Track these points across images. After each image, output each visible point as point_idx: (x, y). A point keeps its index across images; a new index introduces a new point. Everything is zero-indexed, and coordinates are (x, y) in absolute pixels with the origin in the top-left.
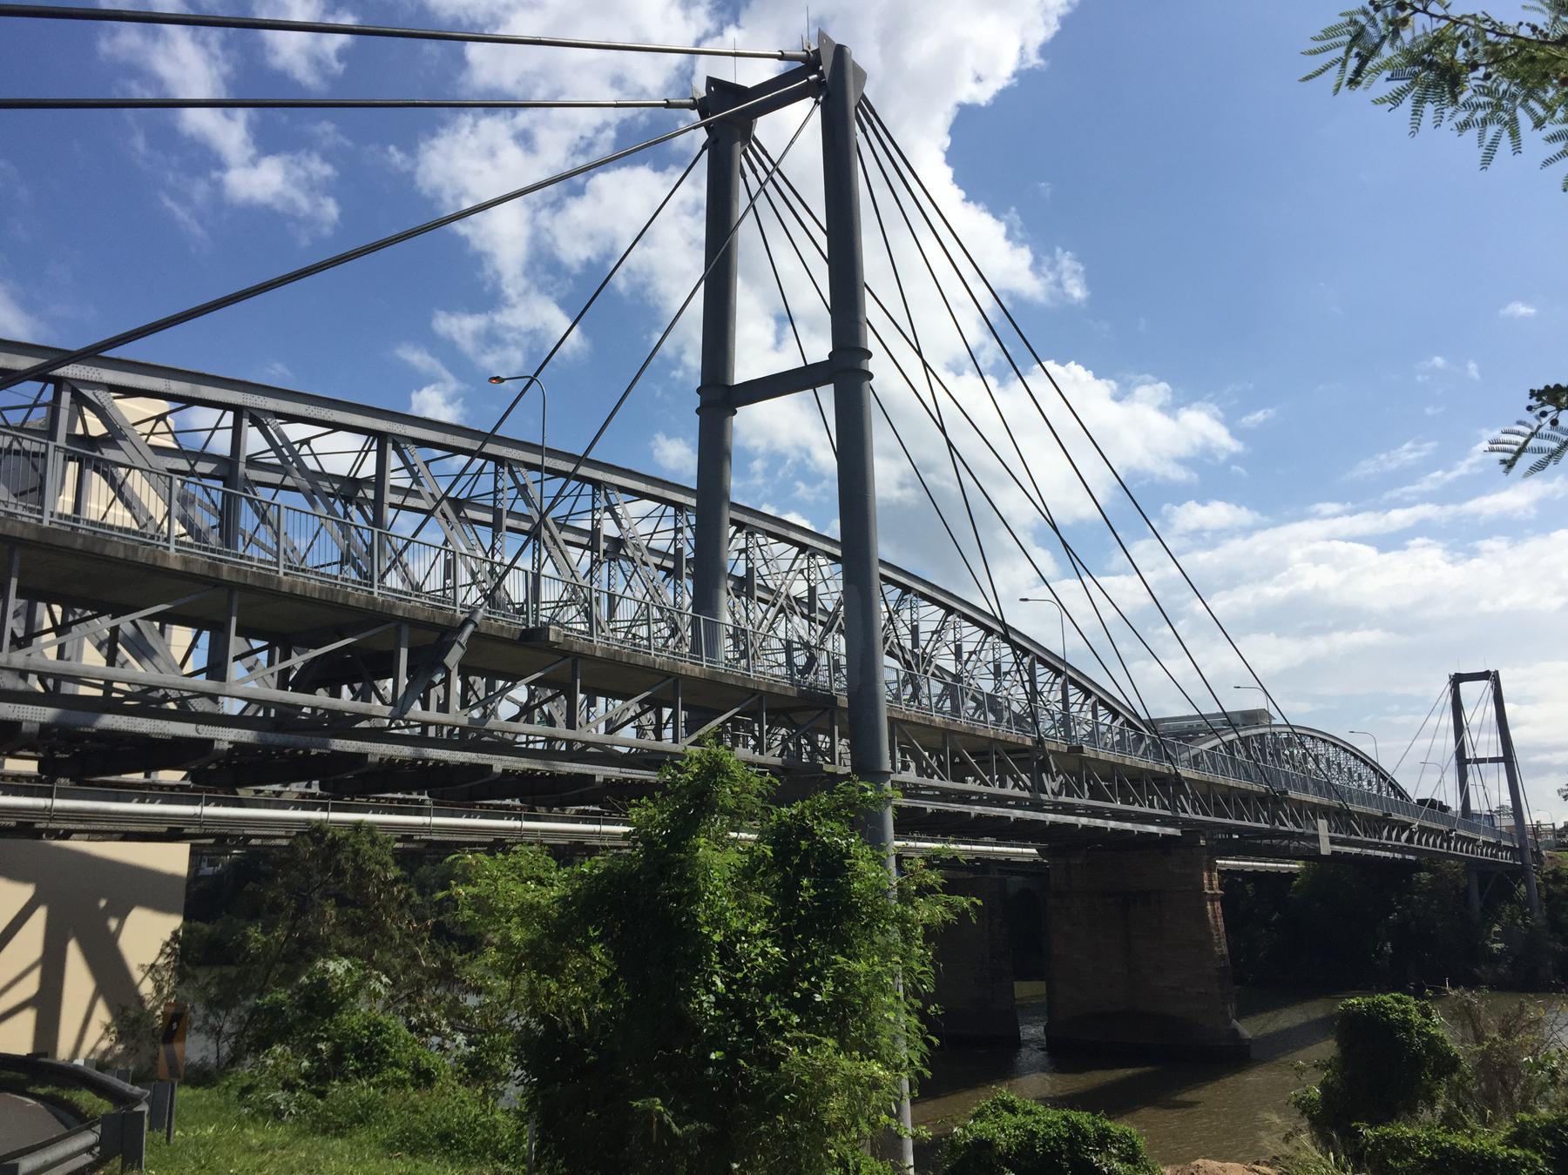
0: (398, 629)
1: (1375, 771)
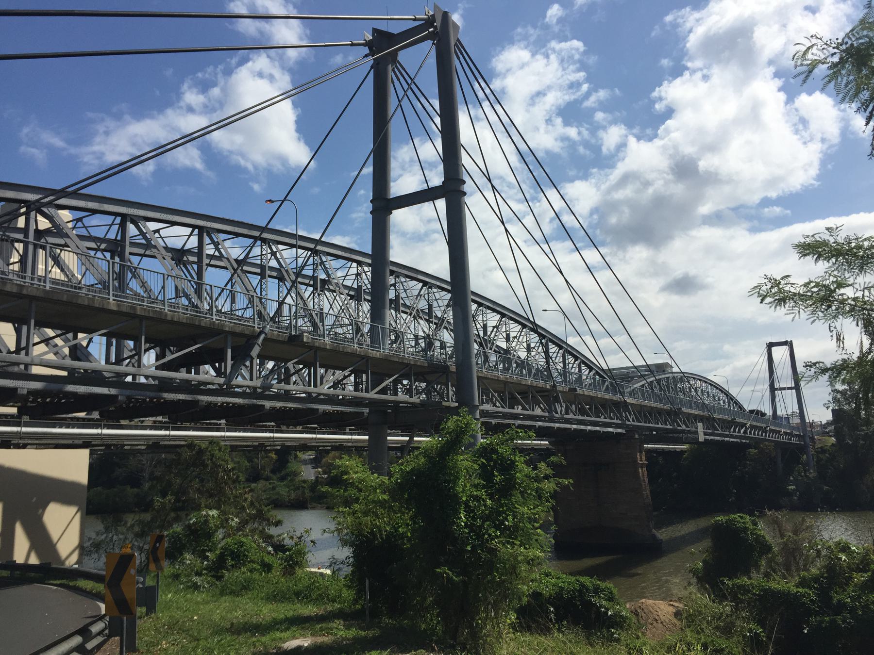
1: (727, 396)
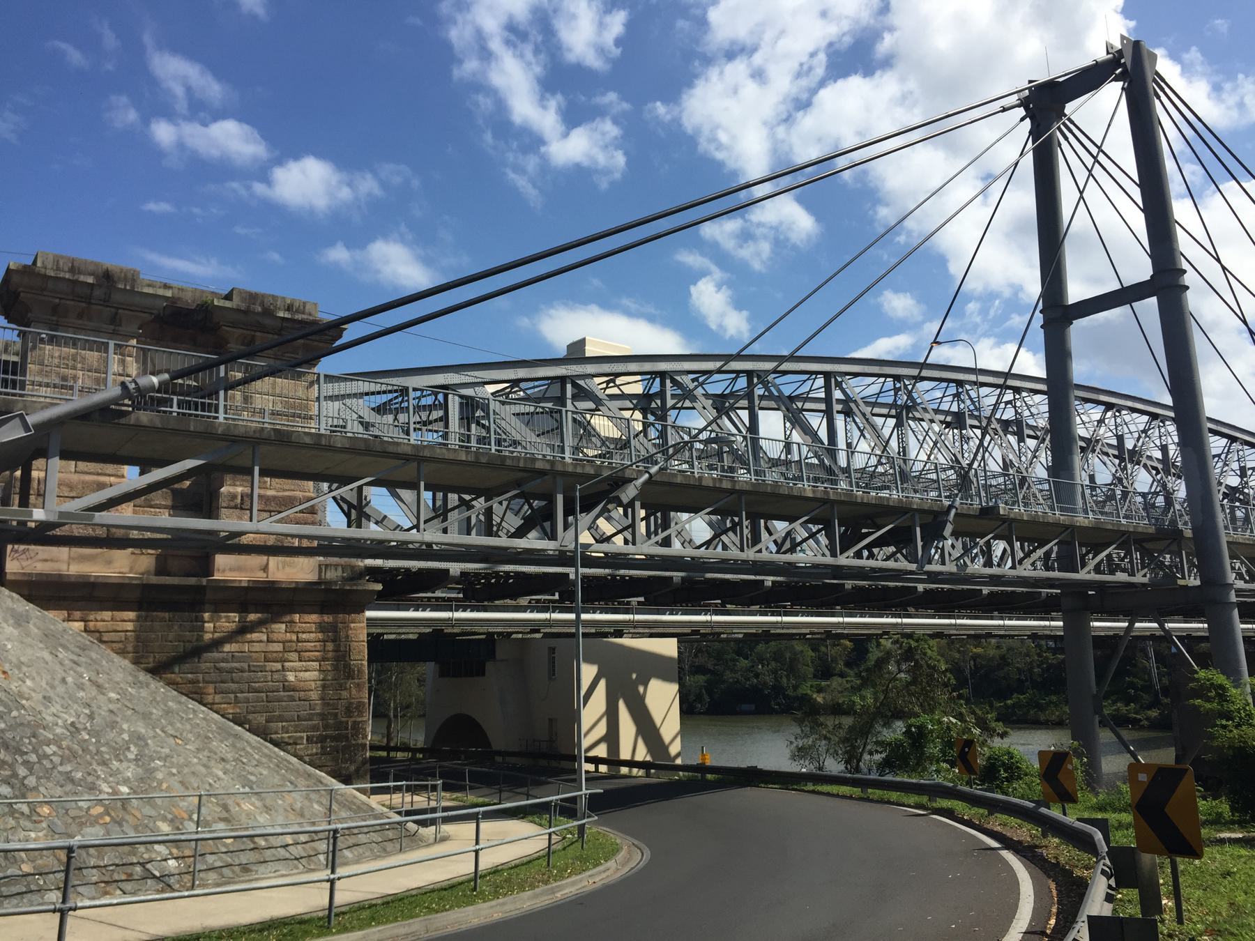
0: (913, 516)
